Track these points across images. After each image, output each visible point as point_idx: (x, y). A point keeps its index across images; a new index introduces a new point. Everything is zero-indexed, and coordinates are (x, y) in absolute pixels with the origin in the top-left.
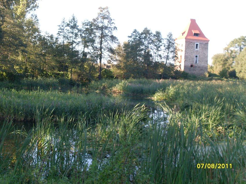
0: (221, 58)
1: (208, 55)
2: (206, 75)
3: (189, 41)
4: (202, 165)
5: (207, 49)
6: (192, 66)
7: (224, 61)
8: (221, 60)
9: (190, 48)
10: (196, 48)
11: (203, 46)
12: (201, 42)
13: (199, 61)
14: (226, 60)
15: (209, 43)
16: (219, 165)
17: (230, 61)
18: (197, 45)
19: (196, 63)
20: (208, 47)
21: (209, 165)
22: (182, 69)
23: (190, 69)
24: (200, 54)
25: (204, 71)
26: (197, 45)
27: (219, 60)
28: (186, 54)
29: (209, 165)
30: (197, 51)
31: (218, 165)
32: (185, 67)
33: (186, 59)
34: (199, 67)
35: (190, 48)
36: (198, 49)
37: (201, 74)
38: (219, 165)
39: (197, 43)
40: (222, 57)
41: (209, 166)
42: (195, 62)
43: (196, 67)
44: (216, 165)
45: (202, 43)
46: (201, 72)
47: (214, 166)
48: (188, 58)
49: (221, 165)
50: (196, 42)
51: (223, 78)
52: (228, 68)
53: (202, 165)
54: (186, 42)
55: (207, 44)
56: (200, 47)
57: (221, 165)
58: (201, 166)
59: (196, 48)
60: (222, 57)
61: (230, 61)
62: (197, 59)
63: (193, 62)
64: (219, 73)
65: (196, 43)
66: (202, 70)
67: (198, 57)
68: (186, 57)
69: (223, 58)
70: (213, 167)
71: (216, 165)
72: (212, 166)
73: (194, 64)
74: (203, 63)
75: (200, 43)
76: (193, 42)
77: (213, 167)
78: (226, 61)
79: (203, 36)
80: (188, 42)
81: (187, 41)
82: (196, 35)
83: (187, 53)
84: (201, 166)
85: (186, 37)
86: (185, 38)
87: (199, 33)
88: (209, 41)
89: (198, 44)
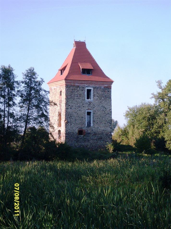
0: (144, 115)
1: (111, 109)
2: (108, 149)
3: (73, 84)
4: (18, 188)
5: (108, 97)
6: (81, 132)
7: (149, 120)
8: (144, 118)
9: (76, 98)
10: (88, 98)
11: (100, 92)
12: (97, 86)
13: (94, 121)
14: (153, 118)
15: (113, 86)
16: (18, 204)
17: (160, 119)
18: (89, 91)
19: (88, 126)
20: (110, 95)
21: (17, 195)
22: (63, 140)
23: (78, 137)
24: (96, 108)
25: (106, 142)
26: (89, 91)
27: (140, 117)
28: (69, 110)
29: (17, 195)
30: (90, 103)
31: (18, 203)
32: (68, 134)
33: (69, 120)
34: (95, 134)
35: (76, 98)
36: (91, 99)
37: (100, 147)
38: (18, 204)
39: (89, 88)
40: (144, 113)
41: (17, 195)
42: (86, 125)
43: (90, 133)
44: (17, 201)
45: (98, 88)
46: (100, 143)
47: (17, 199)
48: (73, 117)
49: (18, 206)
50: (87, 87)
51: (141, 152)
52: (156, 132)
53: (18, 188)
54: (67, 86)
55: (109, 88)
56: (94, 96)
57: (18, 205)
58: (17, 187)
59: (88, 98)
60: (144, 113)
61: (160, 119)
62: (90, 118)
63: (84, 123)
64: (135, 144)
65: (86, 88)
66: (101, 139)
67: (92, 114)
68: (68, 116)
69: (146, 113)
70: (16, 198)
71: (17, 201)
72: (17, 197)
73: (85, 128)
74: (101, 126)
75: (94, 88)
76: (81, 85)
77: (16, 198)
78: (152, 119)
79: (100, 73)
80: (72, 87)
81: (69, 84)
82: (86, 71)
83: (71, 108)
84: (17, 187)
85: (67, 77)
86: (66, 79)
87: (92, 68)
88: (112, 82)
89: (92, 89)
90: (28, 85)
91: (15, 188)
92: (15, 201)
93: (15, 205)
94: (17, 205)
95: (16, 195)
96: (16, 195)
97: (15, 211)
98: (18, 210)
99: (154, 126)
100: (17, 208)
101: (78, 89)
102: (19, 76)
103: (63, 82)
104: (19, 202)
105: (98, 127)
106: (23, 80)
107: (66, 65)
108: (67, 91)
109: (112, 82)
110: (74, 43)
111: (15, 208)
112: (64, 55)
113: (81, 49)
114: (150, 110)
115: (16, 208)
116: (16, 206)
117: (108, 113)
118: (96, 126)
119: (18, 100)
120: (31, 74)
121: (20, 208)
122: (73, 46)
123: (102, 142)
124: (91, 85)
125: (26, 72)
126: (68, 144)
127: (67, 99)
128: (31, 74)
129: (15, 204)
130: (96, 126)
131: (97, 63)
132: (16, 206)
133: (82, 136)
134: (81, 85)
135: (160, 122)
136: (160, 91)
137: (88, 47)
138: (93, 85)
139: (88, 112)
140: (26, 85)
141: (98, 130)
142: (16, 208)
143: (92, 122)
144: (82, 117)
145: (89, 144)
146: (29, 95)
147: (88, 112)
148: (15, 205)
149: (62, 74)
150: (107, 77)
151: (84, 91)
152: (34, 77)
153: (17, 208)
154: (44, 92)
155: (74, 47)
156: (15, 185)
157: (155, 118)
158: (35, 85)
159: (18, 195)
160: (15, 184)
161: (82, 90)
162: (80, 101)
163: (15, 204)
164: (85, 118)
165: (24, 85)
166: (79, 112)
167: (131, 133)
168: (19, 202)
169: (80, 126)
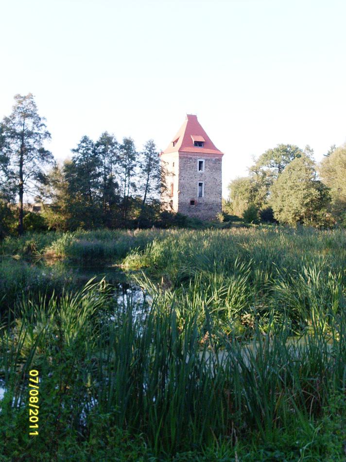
4: (35, 379)
6: (192, 202)
7: (251, 192)
8: (246, 190)
10: (200, 170)
11: (211, 164)
12: (209, 158)
15: (223, 158)
16: (36, 412)
18: (201, 163)
22: (176, 209)
24: (207, 179)
25: (216, 212)
26: (201, 163)
28: (182, 181)
30: (202, 174)
31: (36, 410)
34: (206, 204)
35: (189, 169)
36: (203, 171)
37: (211, 217)
38: (36, 412)
40: (247, 185)
42: (198, 196)
43: (201, 204)
44: (35, 406)
45: (209, 160)
46: (210, 213)
47: (34, 401)
49: (36, 416)
53: (35, 379)
54: (180, 158)
55: (220, 160)
56: (206, 167)
57: (36, 414)
58: (34, 378)
61: (262, 191)
62: (201, 189)
63: (196, 194)
66: (211, 209)
67: (203, 185)
70: (32, 400)
71: (35, 406)
72: (34, 398)
73: (196, 199)
75: (206, 160)
77: (32, 400)
79: (213, 147)
80: (184, 157)
82: (199, 144)
84: (34, 378)
90: (148, 156)
91: (31, 380)
92: (30, 405)
93: (30, 414)
94: (34, 413)
95: (33, 393)
96: (33, 393)
97: (31, 427)
98: (36, 423)
99: (257, 198)
100: (35, 419)
101: (191, 160)
102: (139, 147)
103: (177, 154)
104: (38, 407)
105: (210, 198)
106: (143, 151)
107: (177, 138)
108: (180, 163)
109: (105, 134)
110: (186, 116)
111: (31, 420)
112: (179, 128)
113: (193, 124)
114: (252, 182)
115: (33, 419)
116: (33, 415)
117: (219, 185)
118: (207, 197)
119: (137, 170)
120: (151, 146)
121: (40, 419)
122: (185, 119)
123: (212, 212)
124: (203, 157)
125: (146, 144)
126: (182, 213)
127: (181, 170)
128: (151, 146)
129: (31, 411)
130: (207, 197)
131: (204, 132)
132: (33, 415)
133: (194, 206)
134: (194, 157)
135: (262, 194)
136: (254, 164)
137: (199, 120)
138: (205, 157)
139: (200, 183)
140: (146, 156)
141: (209, 200)
142: (33, 419)
143: (203, 193)
144: (194, 188)
145: (200, 214)
146: (149, 165)
147: (200, 183)
148: (30, 414)
149: (174, 146)
150: (218, 150)
151: (196, 163)
152: (153, 148)
153: (35, 419)
154: (163, 163)
155: (186, 119)
156: (31, 374)
157: (257, 190)
158: (155, 156)
159: (37, 394)
160: (31, 372)
161: (195, 162)
162: (192, 172)
163: (31, 411)
164: (197, 189)
165: (143, 156)
166: (191, 183)
167: (235, 204)
168: (38, 407)
169: (192, 196)
